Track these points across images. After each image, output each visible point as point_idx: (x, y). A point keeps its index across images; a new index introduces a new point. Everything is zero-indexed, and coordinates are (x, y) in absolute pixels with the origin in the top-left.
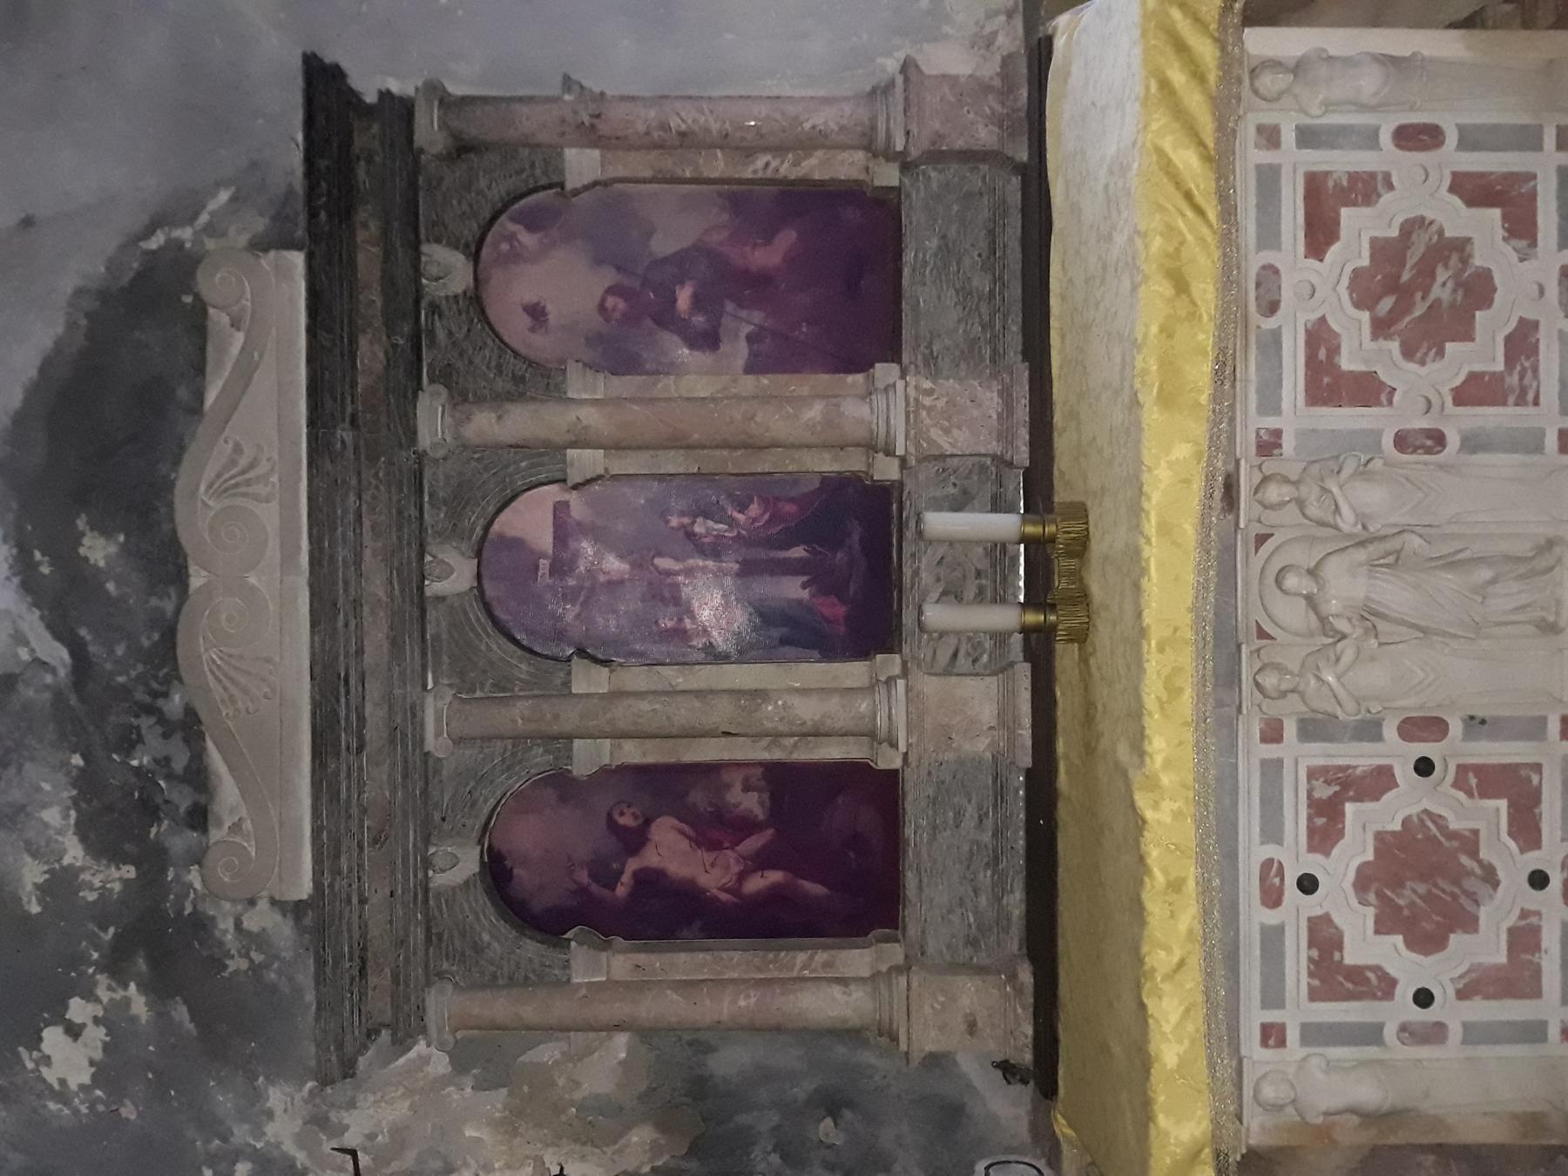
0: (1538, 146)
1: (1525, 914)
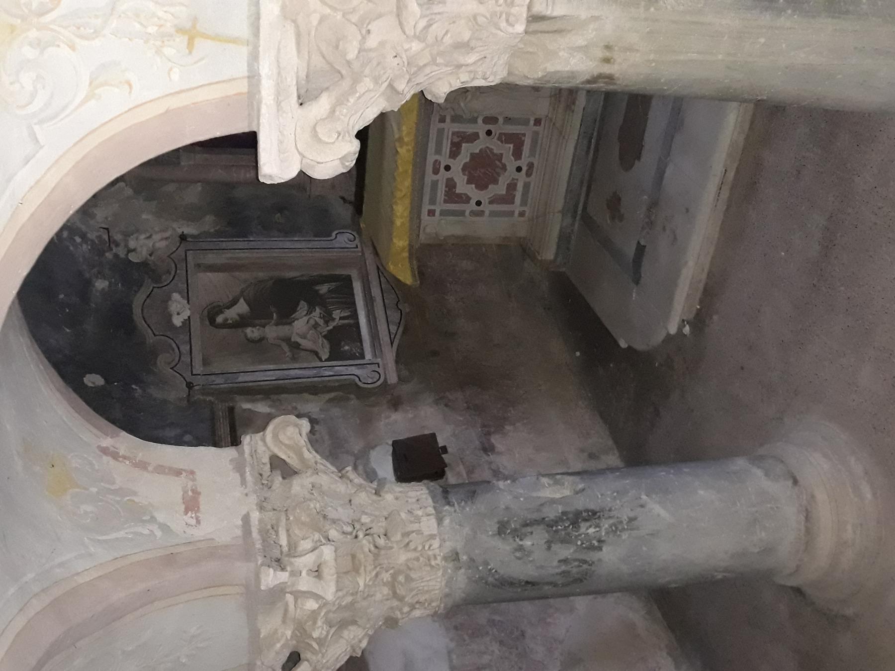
1: (513, 179)
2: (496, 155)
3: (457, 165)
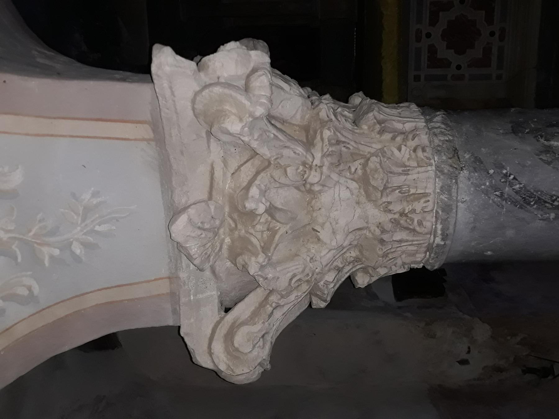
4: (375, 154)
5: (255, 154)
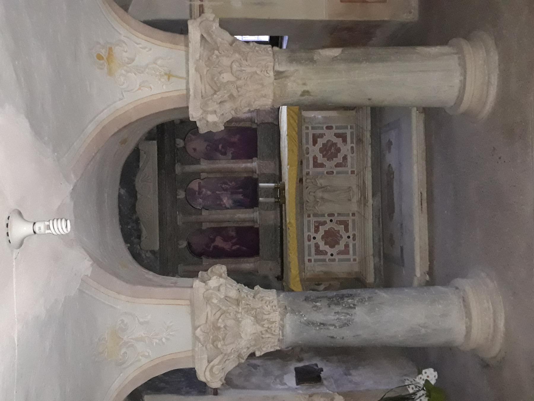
0: (347, 129)
1: (347, 242)
2: (336, 231)
3: (319, 236)
4: (259, 308)
5: (220, 309)
